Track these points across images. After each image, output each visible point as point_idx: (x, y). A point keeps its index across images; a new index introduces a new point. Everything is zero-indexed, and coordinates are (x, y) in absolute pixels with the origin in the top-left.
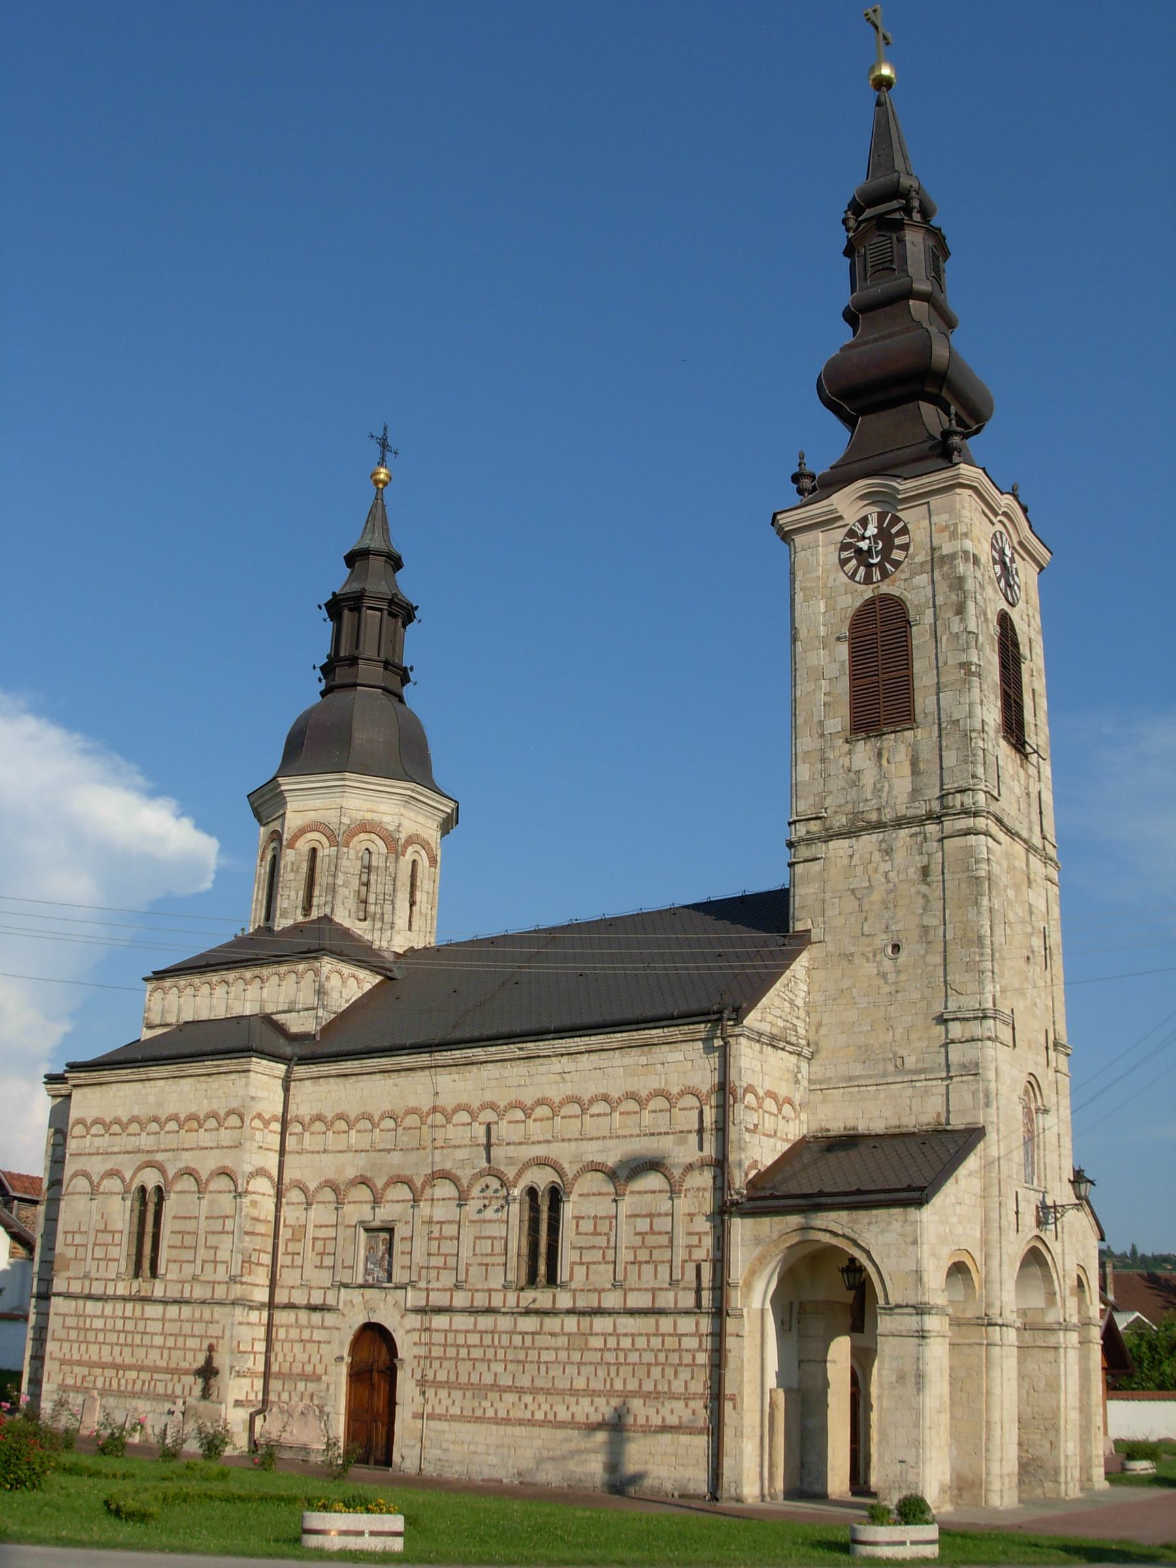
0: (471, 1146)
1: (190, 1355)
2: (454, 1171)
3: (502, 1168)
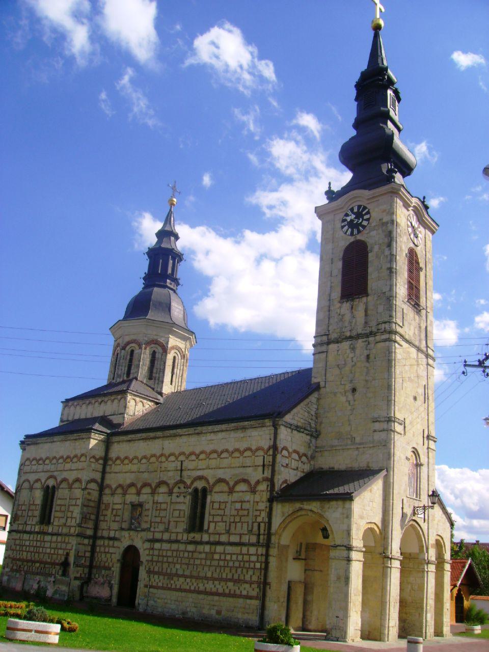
2: (167, 481)
3: (185, 480)
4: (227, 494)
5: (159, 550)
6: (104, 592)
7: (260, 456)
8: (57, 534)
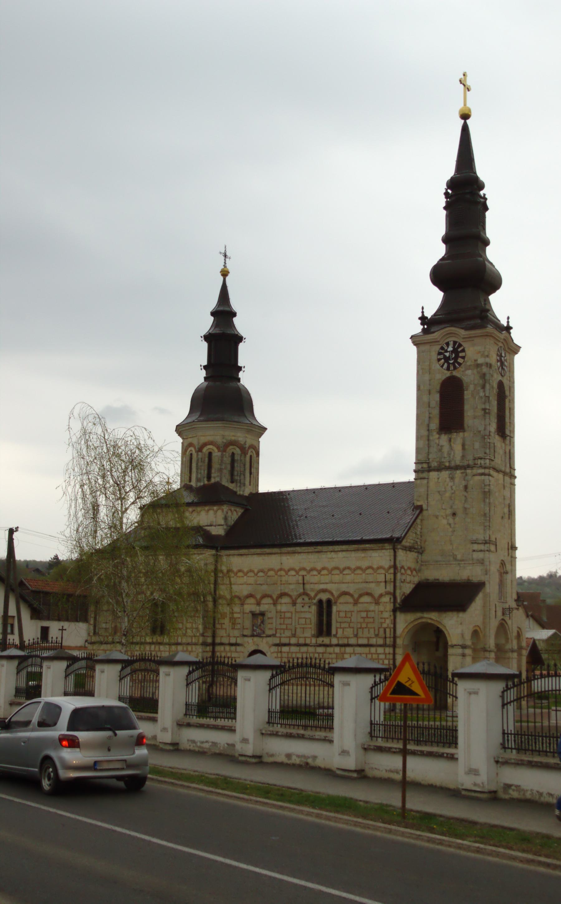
3: (309, 592)
4: (352, 605)
5: (288, 653)
7: (382, 574)
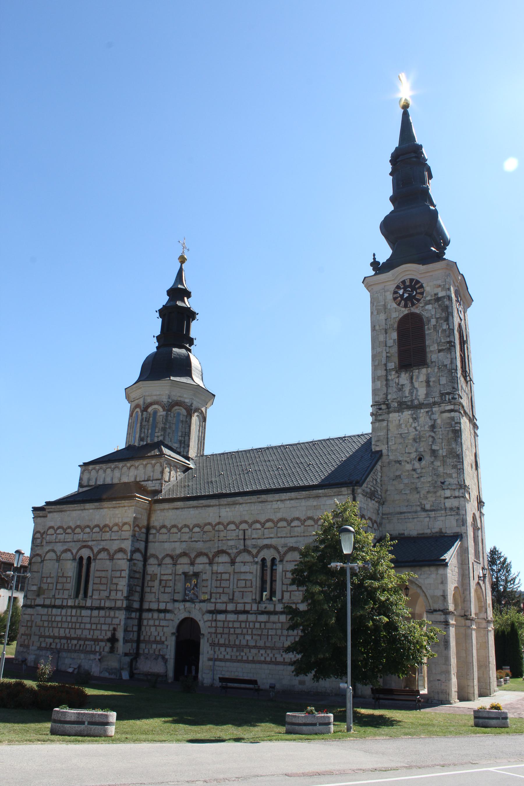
0: (236, 539)
1: (104, 633)
3: (250, 549)
5: (224, 621)
6: (158, 668)
8: (99, 608)
